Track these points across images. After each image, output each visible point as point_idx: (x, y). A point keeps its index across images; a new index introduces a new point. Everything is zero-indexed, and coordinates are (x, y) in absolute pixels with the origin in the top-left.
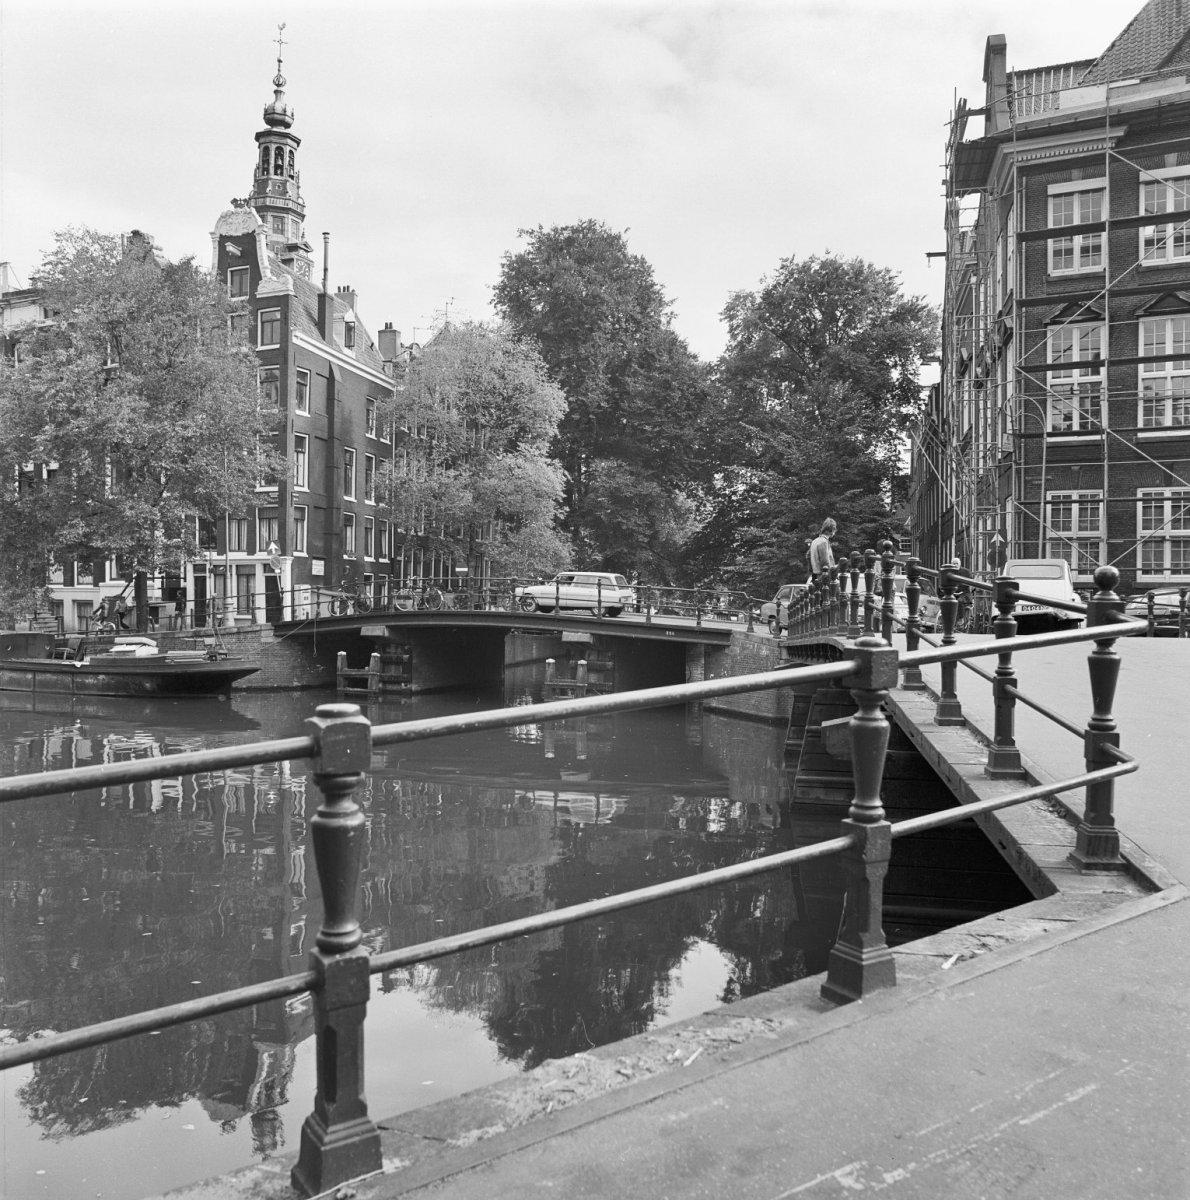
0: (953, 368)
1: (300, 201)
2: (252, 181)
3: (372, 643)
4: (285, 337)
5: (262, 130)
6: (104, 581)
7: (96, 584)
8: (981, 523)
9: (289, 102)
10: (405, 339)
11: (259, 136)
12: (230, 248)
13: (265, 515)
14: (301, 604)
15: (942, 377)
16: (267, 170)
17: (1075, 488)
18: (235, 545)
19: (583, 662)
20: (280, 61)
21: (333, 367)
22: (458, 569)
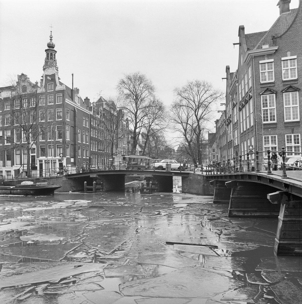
0: (230, 106)
1: (57, 67)
2: (44, 62)
3: (93, 179)
4: (64, 100)
5: (47, 49)
6: (14, 165)
7: (12, 166)
8: (242, 144)
9: (54, 42)
10: (91, 101)
11: (46, 50)
12: (48, 78)
13: (59, 147)
14: (72, 170)
15: (226, 108)
16: (48, 59)
17: (270, 135)
18: (50, 155)
19: (151, 182)
20: (51, 32)
21: (75, 108)
22: (110, 160)
